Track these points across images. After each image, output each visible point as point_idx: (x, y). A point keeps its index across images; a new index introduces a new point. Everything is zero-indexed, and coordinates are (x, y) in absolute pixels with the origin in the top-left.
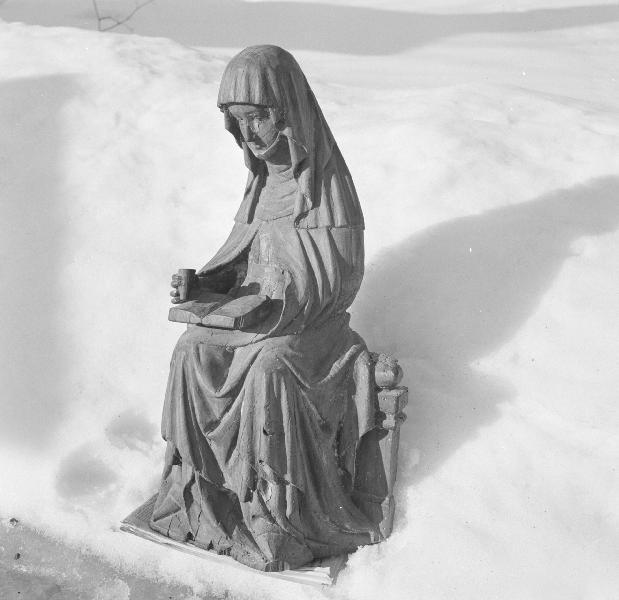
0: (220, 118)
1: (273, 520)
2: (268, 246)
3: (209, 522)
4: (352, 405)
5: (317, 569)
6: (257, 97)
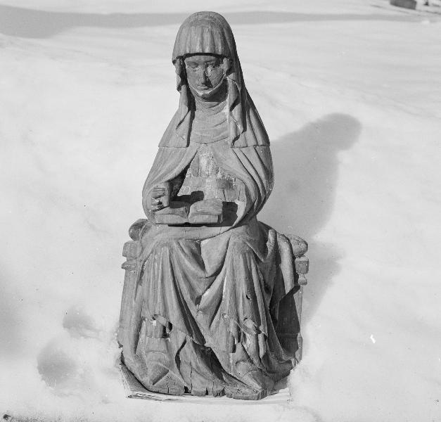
0: (172, 73)
1: (252, 362)
2: (208, 163)
3: (202, 375)
4: (279, 271)
5: (281, 391)
6: (220, 50)
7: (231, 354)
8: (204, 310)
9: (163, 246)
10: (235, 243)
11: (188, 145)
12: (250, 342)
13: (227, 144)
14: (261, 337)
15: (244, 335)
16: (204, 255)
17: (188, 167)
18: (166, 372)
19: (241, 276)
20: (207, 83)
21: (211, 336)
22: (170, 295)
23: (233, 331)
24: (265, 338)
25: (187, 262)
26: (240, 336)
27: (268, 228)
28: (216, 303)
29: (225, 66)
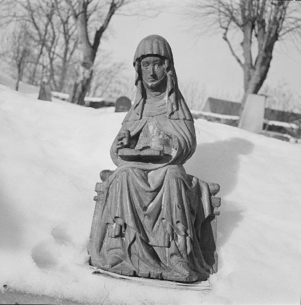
1: (182, 256)
3: (147, 261)
7: (167, 249)
8: (149, 215)
9: (122, 172)
10: (171, 172)
11: (141, 118)
12: (180, 239)
13: (166, 117)
14: (188, 238)
15: (176, 235)
16: (149, 181)
17: (141, 131)
18: (122, 261)
19: (175, 193)
20: (154, 76)
21: (153, 237)
22: (125, 194)
23: (168, 229)
24: (191, 241)
25: (138, 182)
26: (173, 236)
27: (193, 176)
28: (158, 209)
29: (165, 66)
